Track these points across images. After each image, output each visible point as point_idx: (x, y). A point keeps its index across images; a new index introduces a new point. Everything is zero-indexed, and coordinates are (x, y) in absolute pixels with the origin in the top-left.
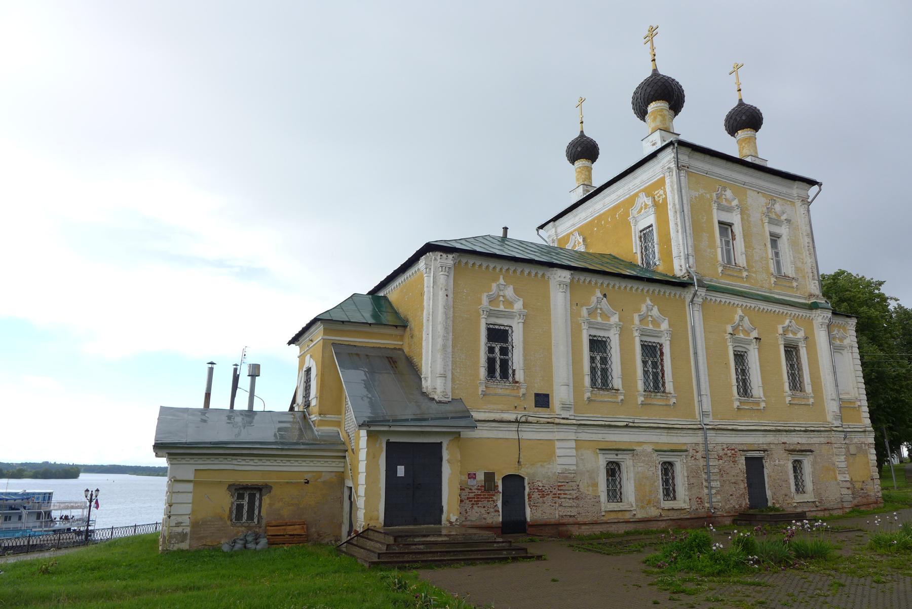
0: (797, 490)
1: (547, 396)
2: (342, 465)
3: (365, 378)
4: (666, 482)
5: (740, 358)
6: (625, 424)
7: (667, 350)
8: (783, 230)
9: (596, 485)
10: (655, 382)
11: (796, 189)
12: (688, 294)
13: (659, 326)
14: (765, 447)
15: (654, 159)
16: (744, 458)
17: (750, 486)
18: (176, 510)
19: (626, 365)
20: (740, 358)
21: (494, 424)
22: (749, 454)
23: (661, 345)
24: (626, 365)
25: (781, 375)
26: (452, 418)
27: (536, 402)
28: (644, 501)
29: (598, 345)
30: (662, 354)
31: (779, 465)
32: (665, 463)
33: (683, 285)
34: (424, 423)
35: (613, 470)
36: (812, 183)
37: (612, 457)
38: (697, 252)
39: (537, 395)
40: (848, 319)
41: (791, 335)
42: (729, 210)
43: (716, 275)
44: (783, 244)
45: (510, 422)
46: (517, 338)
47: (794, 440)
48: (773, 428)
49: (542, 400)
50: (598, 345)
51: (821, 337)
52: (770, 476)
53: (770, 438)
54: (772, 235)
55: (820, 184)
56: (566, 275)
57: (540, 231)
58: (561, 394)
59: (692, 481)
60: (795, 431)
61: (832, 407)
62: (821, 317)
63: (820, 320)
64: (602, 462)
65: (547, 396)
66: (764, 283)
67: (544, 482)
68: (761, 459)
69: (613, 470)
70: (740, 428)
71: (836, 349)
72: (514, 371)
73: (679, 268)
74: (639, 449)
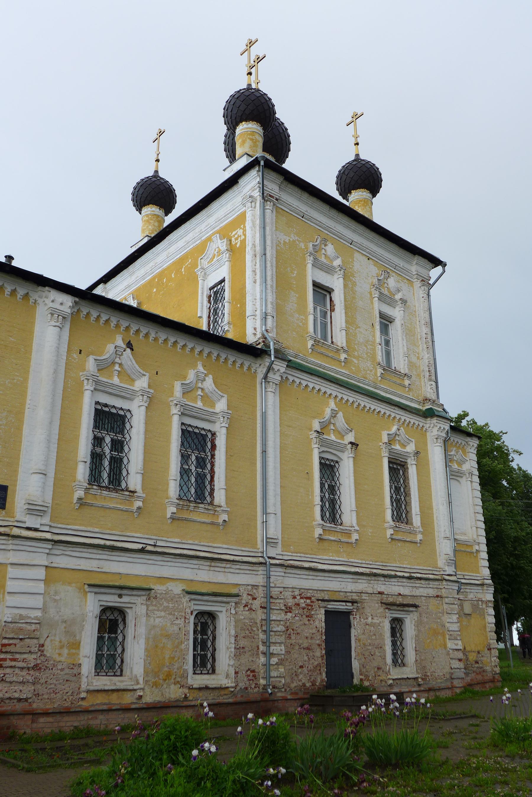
0: (395, 662)
5: (329, 468)
6: (140, 546)
7: (221, 442)
9: (76, 645)
10: (198, 486)
11: (415, 266)
12: (260, 368)
13: (213, 406)
16: (323, 611)
19: (151, 455)
20: (329, 468)
22: (331, 606)
25: (383, 499)
28: (157, 673)
29: (110, 421)
31: (372, 625)
36: (435, 262)
43: (302, 349)
47: (394, 589)
48: (368, 571)
49: (281, 593)
50: (110, 421)
51: (436, 454)
53: (362, 585)
55: (444, 265)
59: (242, 643)
60: (396, 576)
61: (444, 549)
63: (435, 432)
66: (368, 374)
68: (347, 614)
70: (320, 567)
71: (453, 475)
73: (251, 338)
74: (159, 588)
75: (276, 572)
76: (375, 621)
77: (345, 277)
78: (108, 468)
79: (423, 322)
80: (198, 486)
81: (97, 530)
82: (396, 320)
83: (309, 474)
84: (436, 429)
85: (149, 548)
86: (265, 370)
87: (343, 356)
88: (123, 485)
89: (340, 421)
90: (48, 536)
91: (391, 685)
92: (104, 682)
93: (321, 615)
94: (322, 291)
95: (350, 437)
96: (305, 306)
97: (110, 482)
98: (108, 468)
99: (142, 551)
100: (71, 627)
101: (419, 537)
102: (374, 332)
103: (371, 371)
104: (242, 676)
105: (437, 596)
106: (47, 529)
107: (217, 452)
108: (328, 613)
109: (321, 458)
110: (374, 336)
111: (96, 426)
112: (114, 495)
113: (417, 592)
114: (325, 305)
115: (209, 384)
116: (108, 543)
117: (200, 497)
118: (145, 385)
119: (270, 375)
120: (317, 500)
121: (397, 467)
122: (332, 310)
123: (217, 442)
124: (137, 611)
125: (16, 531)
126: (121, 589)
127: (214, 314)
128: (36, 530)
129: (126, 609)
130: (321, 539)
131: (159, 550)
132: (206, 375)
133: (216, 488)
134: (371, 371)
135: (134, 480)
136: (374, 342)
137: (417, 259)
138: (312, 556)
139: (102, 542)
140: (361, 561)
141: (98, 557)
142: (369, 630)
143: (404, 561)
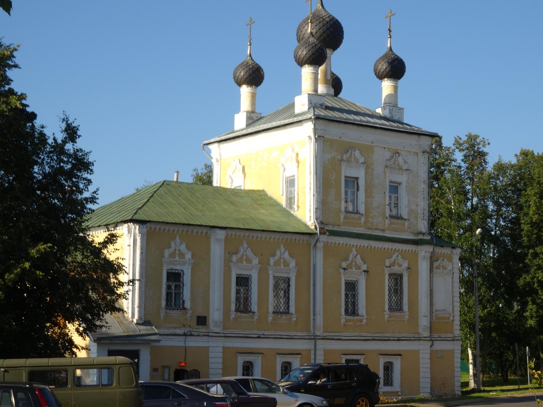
6: (257, 336)
29: (243, 281)
66: (381, 224)
77: (367, 168)
78: (243, 305)
79: (422, 180)
81: (356, 334)
82: (403, 183)
83: (339, 292)
84: (423, 252)
85: (262, 336)
86: (315, 241)
88: (249, 309)
90: (223, 335)
96: (340, 195)
97: (244, 309)
98: (243, 305)
99: (259, 337)
102: (385, 197)
103: (381, 223)
106: (221, 332)
107: (290, 288)
110: (385, 200)
112: (246, 315)
114: (354, 188)
116: (245, 335)
118: (257, 263)
119: (318, 244)
120: (387, 288)
121: (397, 279)
122: (358, 190)
123: (291, 283)
125: (211, 334)
128: (218, 333)
129: (313, 11)
130: (345, 325)
131: (265, 336)
132: (285, 251)
133: (290, 305)
134: (381, 223)
135: (254, 307)
136: (385, 204)
137: (423, 138)
138: (337, 334)
139: (242, 335)
141: (55, 368)
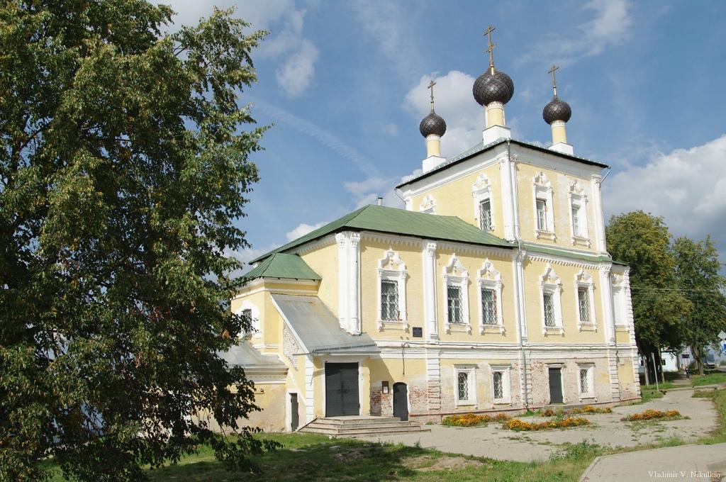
0: (582, 391)
1: (421, 329)
2: (438, 372)
3: (713, 407)
4: (496, 386)
5: (547, 298)
7: (498, 294)
8: (581, 203)
9: (452, 388)
10: (489, 314)
12: (513, 254)
13: (493, 278)
14: (562, 361)
15: (492, 150)
16: (548, 368)
17: (551, 387)
18: (375, 385)
19: (470, 304)
20: (547, 298)
21: (387, 349)
22: (552, 366)
23: (495, 291)
24: (470, 304)
26: (365, 346)
27: (414, 333)
28: (481, 399)
29: (453, 293)
30: (495, 297)
31: (571, 373)
32: (496, 373)
33: (511, 248)
34: (349, 350)
35: (462, 378)
37: (463, 370)
38: (518, 227)
39: (414, 329)
40: (624, 268)
41: (582, 281)
42: (544, 189)
43: (530, 237)
44: (580, 213)
45: (398, 347)
46: (401, 289)
47: (580, 355)
49: (418, 332)
50: (453, 293)
51: (604, 282)
52: (564, 381)
53: (566, 355)
54: (573, 206)
56: (432, 245)
57: (398, 190)
58: (428, 331)
59: (513, 385)
61: (608, 334)
62: (603, 269)
63: (604, 269)
64: (454, 374)
65: (421, 329)
66: (566, 243)
67: (419, 387)
68: (559, 369)
69: (462, 378)
70: (546, 348)
71: (614, 290)
72: (399, 312)
73: (509, 235)
74: (479, 364)
75: (527, 352)
76: (573, 371)
80: (489, 314)
87: (553, 237)
89: (552, 274)
90: (438, 346)
91: (581, 401)
92: (462, 402)
93: (547, 371)
94: (540, 203)
95: (558, 282)
100: (449, 381)
101: (595, 328)
104: (514, 398)
105: (605, 357)
108: (550, 369)
109: (544, 293)
111: (449, 296)
113: (594, 356)
115: (491, 268)
117: (491, 322)
124: (472, 374)
126: (466, 366)
127: (486, 221)
140: (566, 342)
142: (569, 378)
143: (588, 340)
